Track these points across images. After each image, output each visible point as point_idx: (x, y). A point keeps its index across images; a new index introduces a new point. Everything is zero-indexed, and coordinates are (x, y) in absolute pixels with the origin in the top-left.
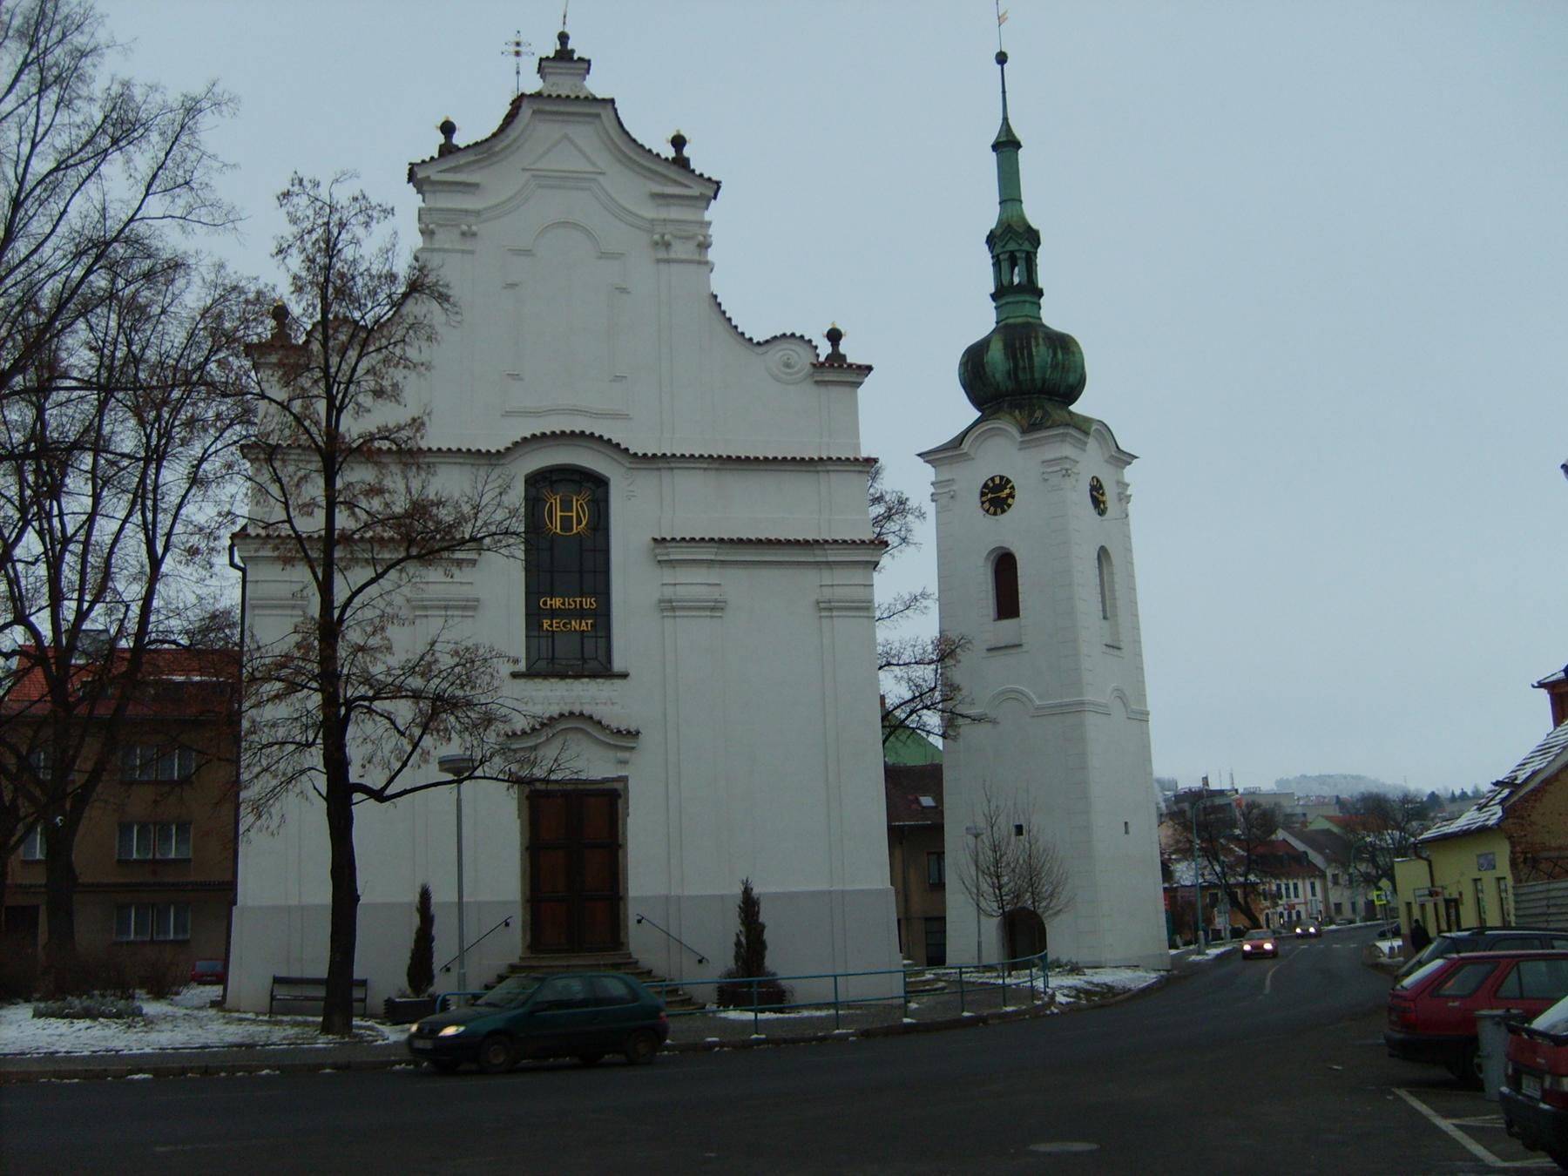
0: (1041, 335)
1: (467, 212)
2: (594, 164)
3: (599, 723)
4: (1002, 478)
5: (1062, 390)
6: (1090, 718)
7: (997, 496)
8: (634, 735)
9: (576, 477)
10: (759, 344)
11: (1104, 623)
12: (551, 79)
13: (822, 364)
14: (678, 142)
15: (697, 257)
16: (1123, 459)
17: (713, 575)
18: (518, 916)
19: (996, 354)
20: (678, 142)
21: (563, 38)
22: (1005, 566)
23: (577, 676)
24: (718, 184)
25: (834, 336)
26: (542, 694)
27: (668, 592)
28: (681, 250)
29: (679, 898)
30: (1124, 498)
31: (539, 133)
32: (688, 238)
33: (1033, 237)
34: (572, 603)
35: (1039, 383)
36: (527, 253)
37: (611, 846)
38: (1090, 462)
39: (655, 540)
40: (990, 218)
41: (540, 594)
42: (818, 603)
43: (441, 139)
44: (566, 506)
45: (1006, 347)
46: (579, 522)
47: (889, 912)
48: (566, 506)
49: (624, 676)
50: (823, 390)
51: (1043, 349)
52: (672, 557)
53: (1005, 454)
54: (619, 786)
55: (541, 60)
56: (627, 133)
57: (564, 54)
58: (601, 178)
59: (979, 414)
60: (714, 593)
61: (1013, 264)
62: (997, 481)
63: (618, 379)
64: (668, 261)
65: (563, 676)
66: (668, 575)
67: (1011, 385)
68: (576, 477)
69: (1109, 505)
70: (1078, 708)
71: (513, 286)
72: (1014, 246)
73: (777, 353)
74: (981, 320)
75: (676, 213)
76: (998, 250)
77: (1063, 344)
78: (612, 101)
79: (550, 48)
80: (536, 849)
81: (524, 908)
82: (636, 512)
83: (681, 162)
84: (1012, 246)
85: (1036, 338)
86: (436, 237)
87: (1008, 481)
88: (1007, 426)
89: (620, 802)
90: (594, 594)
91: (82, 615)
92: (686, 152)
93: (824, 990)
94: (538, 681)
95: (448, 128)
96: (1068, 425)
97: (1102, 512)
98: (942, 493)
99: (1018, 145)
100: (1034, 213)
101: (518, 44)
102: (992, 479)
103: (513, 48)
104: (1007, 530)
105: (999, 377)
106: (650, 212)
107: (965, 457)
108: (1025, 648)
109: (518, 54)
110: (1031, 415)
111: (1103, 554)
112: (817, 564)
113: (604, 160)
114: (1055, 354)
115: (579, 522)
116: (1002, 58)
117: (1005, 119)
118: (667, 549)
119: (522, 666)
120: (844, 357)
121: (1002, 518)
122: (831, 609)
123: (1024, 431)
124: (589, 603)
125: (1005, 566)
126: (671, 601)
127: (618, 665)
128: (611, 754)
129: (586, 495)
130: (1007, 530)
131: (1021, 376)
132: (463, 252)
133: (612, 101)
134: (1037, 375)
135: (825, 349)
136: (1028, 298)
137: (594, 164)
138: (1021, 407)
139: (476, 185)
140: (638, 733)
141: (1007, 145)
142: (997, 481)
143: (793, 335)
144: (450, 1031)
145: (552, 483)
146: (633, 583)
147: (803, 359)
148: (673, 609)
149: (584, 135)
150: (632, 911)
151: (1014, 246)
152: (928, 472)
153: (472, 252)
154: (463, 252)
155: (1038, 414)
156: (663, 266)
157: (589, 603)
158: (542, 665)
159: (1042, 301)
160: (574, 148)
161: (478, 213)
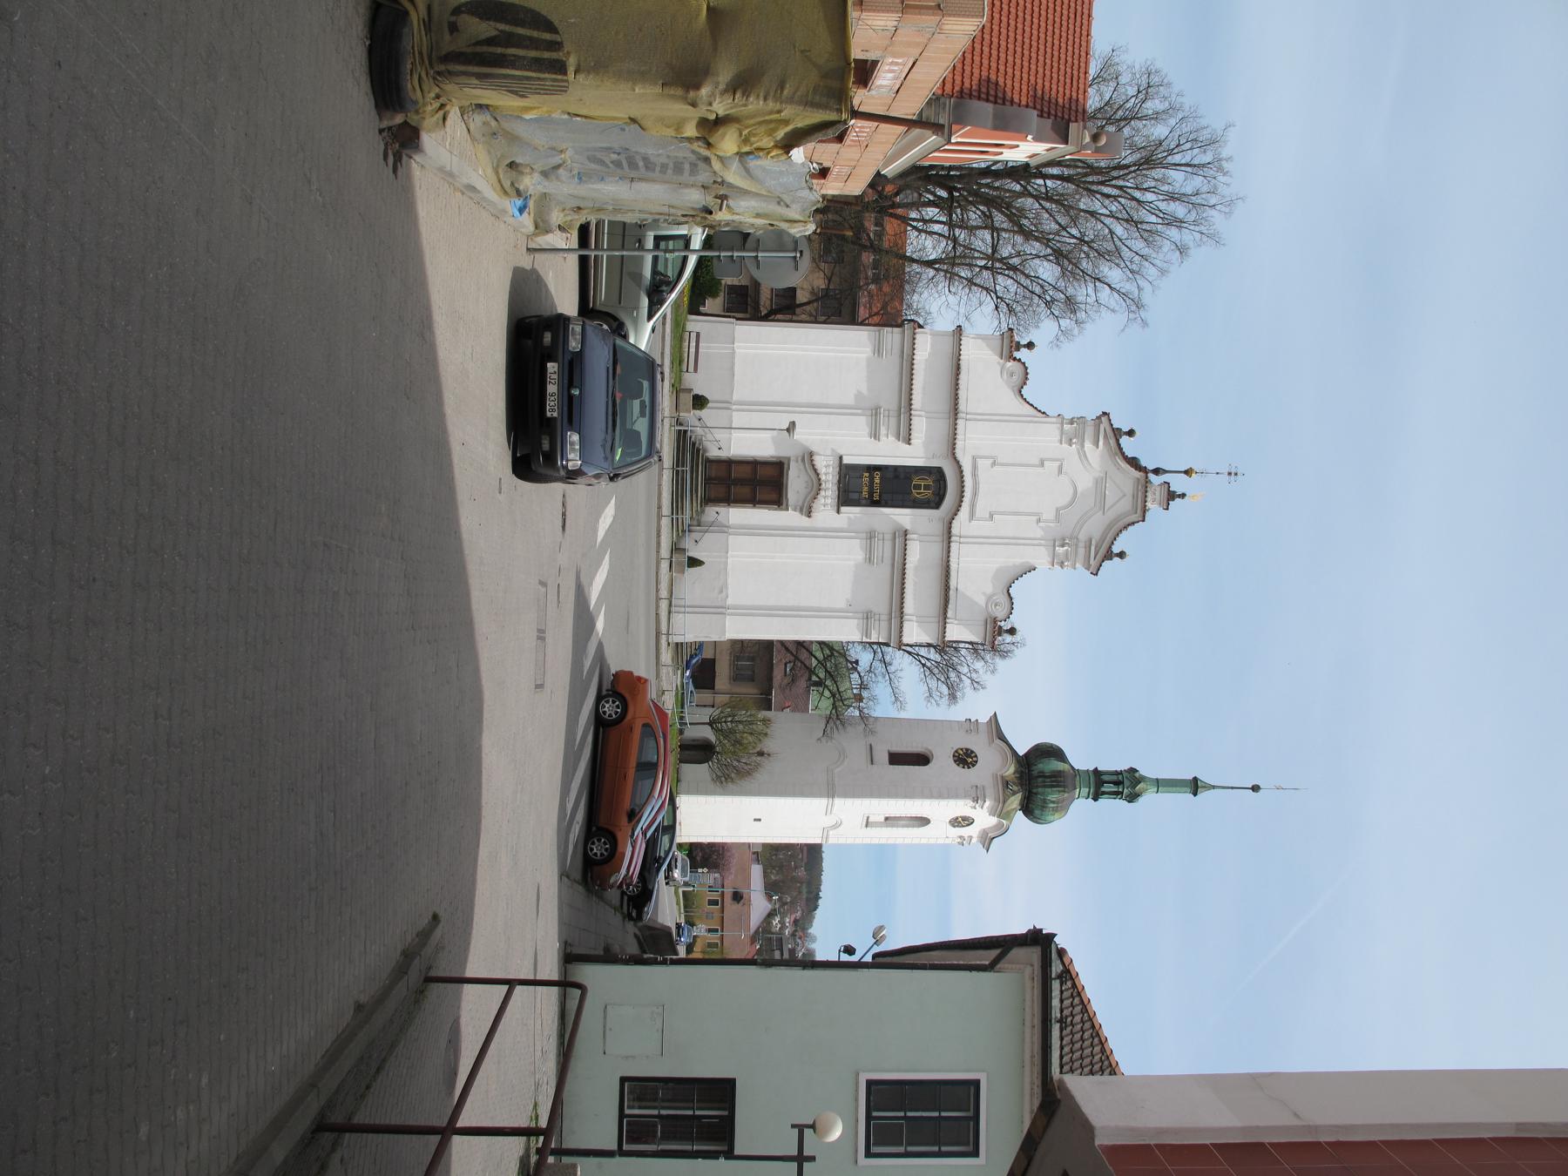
7: (965, 758)
8: (809, 515)
14: (1121, 555)
16: (987, 840)
17: (888, 560)
18: (723, 454)
19: (1060, 766)
22: (922, 759)
33: (1132, 798)
37: (753, 501)
43: (1125, 429)
44: (927, 487)
53: (992, 765)
59: (1021, 751)
66: (888, 536)
67: (1035, 773)
72: (1121, 785)
73: (1004, 599)
74: (1081, 758)
75: (1081, 551)
77: (1062, 808)
80: (755, 464)
83: (1109, 555)
84: (1127, 783)
91: (915, 228)
95: (1131, 433)
98: (971, 726)
105: (1040, 766)
106: (1083, 536)
113: (1111, 515)
116: (1255, 788)
119: (846, 461)
124: (876, 497)
125: (922, 759)
127: (843, 509)
135: (1006, 626)
141: (1195, 786)
144: (144, 1130)
147: (1000, 613)
149: (1125, 505)
151: (1121, 785)
152: (984, 718)
157: (876, 497)
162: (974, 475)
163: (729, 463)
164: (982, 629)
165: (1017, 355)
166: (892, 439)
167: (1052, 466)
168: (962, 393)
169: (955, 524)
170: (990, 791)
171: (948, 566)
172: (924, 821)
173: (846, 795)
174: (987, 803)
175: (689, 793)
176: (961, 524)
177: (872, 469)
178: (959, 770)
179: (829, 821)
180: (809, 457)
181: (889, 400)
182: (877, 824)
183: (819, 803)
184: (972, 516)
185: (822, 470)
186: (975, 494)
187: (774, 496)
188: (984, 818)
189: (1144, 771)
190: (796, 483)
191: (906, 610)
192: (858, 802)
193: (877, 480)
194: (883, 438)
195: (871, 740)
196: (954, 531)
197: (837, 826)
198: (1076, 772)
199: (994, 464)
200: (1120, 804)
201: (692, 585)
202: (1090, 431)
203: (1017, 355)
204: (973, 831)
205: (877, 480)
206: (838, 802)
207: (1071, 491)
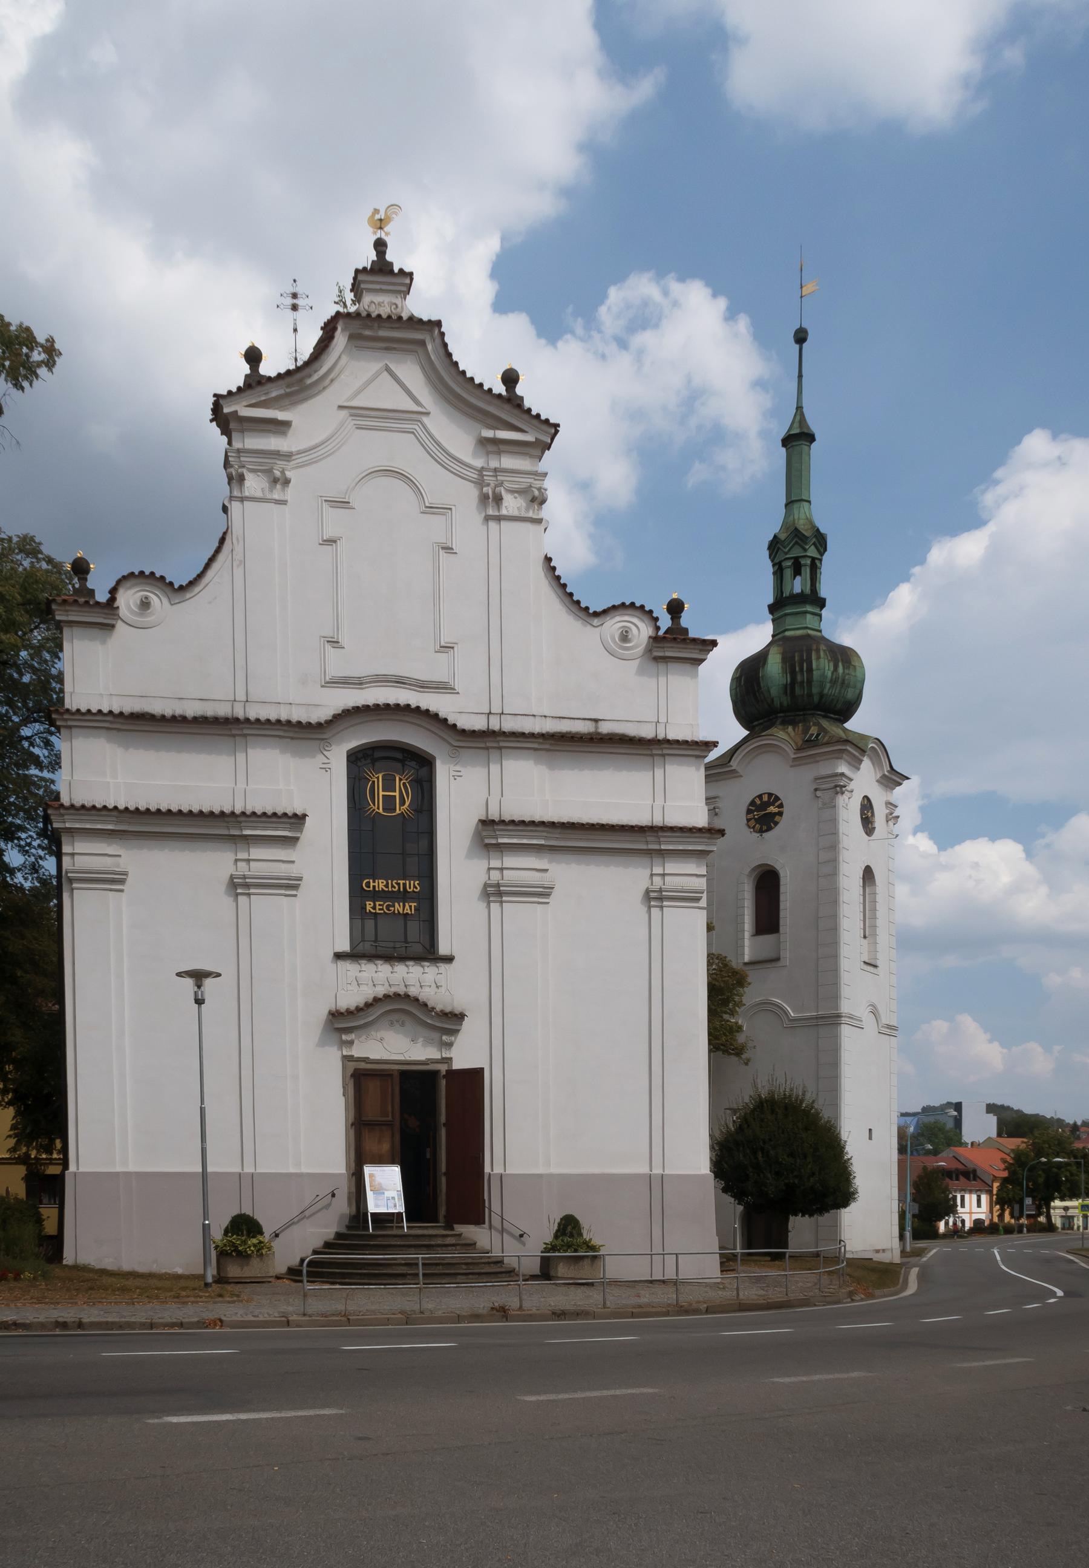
0: (823, 647)
3: (426, 1005)
4: (770, 795)
5: (839, 706)
7: (764, 814)
8: (460, 1017)
9: (399, 756)
11: (865, 942)
13: (663, 639)
14: (510, 378)
19: (774, 666)
20: (510, 378)
21: (380, 246)
24: (556, 426)
25: (675, 608)
27: (495, 876)
28: (512, 504)
33: (821, 542)
35: (816, 699)
36: (344, 504)
43: (246, 369)
44: (389, 785)
45: (784, 660)
46: (403, 803)
48: (389, 785)
49: (449, 959)
50: (662, 666)
52: (501, 841)
53: (774, 773)
55: (357, 271)
61: (797, 571)
62: (765, 798)
63: (447, 648)
64: (499, 519)
67: (786, 701)
69: (876, 825)
71: (331, 541)
73: (614, 625)
77: (844, 656)
78: (439, 324)
79: (367, 257)
81: (349, 1181)
82: (462, 795)
83: (513, 401)
84: (797, 552)
85: (818, 651)
87: (777, 798)
88: (783, 736)
90: (418, 878)
92: (520, 390)
93: (638, 1270)
95: (253, 356)
96: (847, 741)
99: (811, 438)
100: (822, 512)
101: (295, 296)
102: (760, 797)
103: (289, 301)
104: (769, 849)
105: (774, 692)
109: (295, 308)
110: (806, 731)
111: (868, 874)
112: (649, 853)
114: (836, 667)
115: (403, 803)
116: (801, 337)
117: (799, 408)
118: (494, 833)
119: (345, 946)
124: (413, 885)
125: (767, 883)
127: (443, 949)
128: (436, 1035)
130: (769, 849)
131: (798, 691)
133: (439, 324)
134: (815, 690)
135: (665, 622)
136: (809, 608)
138: (794, 723)
139: (287, 424)
142: (765, 798)
145: (374, 761)
147: (642, 631)
155: (814, 730)
156: (492, 525)
157: (413, 885)
158: (367, 947)
159: (824, 612)
161: (288, 456)
162: (358, 683)
165: (102, 597)
167: (334, 522)
168: (191, 710)
170: (824, 769)
171: (543, 736)
173: (835, 997)
174: (843, 768)
176: (462, 709)
177: (358, 895)
179: (868, 1020)
180: (342, 1022)
181: (217, 863)
182: (874, 951)
183: (847, 1033)
184: (443, 687)
185: (367, 993)
186: (400, 682)
188: (863, 780)
189: (773, 526)
190: (395, 1046)
191: (641, 818)
192: (845, 978)
193: (380, 884)
194: (293, 870)
196: (478, 724)
197: (875, 1012)
198: (778, 637)
199: (334, 643)
201: (625, 1252)
202: (253, 442)
203: (102, 597)
205: (380, 884)
206: (845, 1007)
207: (385, 481)
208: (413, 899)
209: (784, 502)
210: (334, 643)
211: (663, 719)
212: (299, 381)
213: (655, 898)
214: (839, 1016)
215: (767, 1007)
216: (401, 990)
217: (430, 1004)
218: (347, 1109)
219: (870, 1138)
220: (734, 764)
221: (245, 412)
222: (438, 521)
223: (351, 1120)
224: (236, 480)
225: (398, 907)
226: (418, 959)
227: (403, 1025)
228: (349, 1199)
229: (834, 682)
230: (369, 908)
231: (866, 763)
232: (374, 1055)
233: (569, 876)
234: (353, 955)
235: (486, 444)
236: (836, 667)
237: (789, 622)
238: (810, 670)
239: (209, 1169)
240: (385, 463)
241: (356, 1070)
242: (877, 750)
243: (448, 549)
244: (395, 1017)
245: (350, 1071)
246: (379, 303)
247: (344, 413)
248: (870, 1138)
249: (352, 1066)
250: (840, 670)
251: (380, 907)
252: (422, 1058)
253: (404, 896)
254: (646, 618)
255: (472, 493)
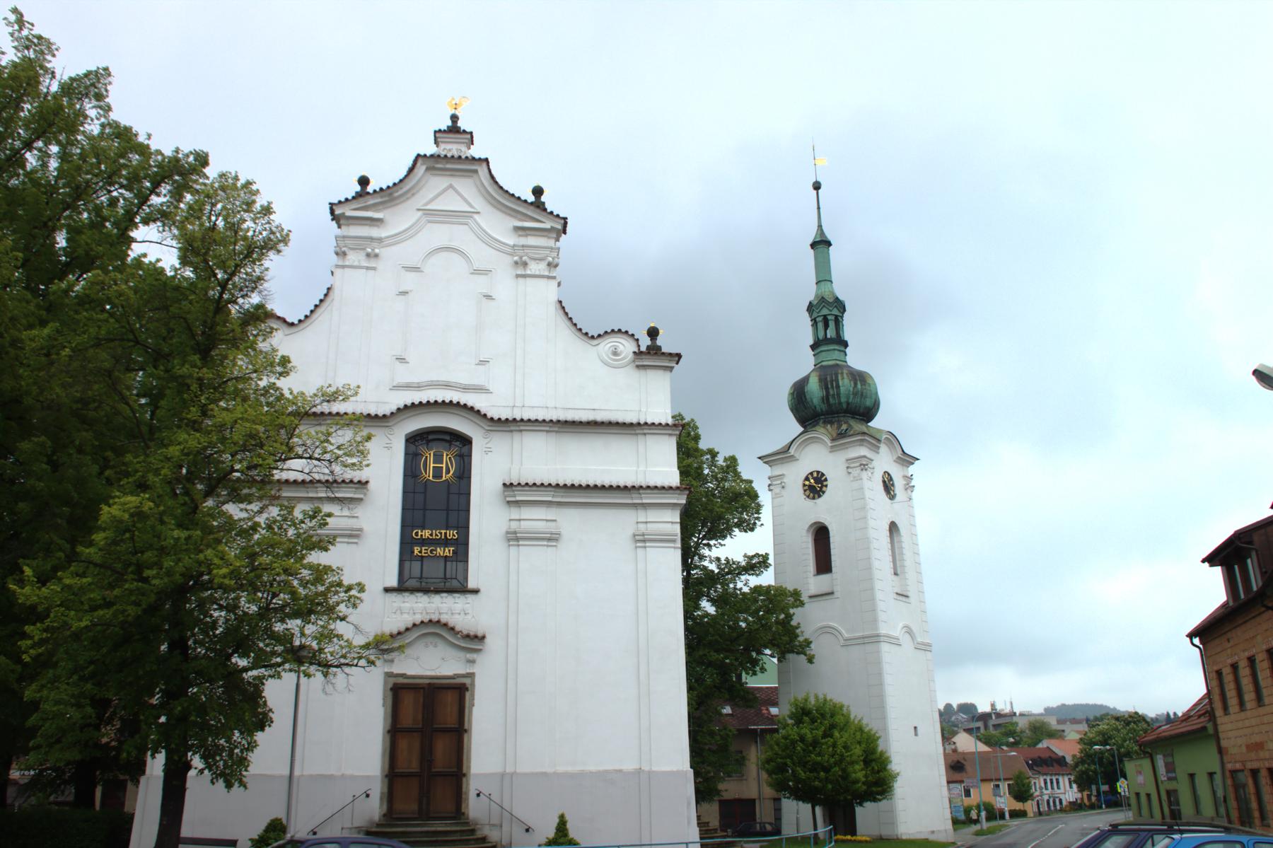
1: (372, 239)
2: (471, 206)
6: (885, 647)
8: (480, 639)
9: (448, 438)
10: (593, 337)
11: (894, 577)
12: (442, 146)
14: (538, 192)
15: (546, 273)
16: (907, 460)
18: (377, 789)
19: (814, 387)
20: (538, 192)
21: (454, 118)
22: (821, 535)
23: (437, 591)
24: (565, 219)
25: (653, 333)
26: (407, 605)
27: (514, 525)
29: (650, 772)
30: (909, 487)
31: (434, 189)
32: (541, 260)
33: (840, 306)
34: (438, 534)
36: (416, 269)
37: (458, 732)
38: (884, 461)
39: (504, 485)
40: (809, 293)
41: (414, 527)
42: (634, 535)
44: (438, 459)
45: (820, 380)
46: (448, 472)
47: (689, 789)
48: (438, 459)
49: (476, 592)
50: (642, 372)
51: (846, 381)
54: (467, 681)
56: (501, 188)
57: (454, 129)
58: (476, 216)
59: (802, 429)
60: (551, 527)
64: (524, 276)
65: (426, 591)
66: (515, 513)
67: (824, 407)
68: (448, 438)
70: (875, 639)
71: (404, 293)
73: (606, 345)
74: (803, 363)
76: (815, 315)
77: (860, 378)
78: (486, 160)
79: (446, 123)
80: (395, 732)
82: (491, 465)
83: (539, 205)
84: (825, 312)
86: (348, 257)
88: (823, 433)
89: (468, 695)
90: (457, 528)
94: (406, 594)
95: (364, 181)
97: (892, 497)
99: (829, 244)
104: (821, 510)
105: (816, 401)
106: (511, 240)
107: (792, 459)
108: (836, 595)
111: (893, 527)
112: (635, 506)
113: (479, 203)
114: (856, 384)
115: (448, 472)
116: (817, 186)
117: (820, 226)
118: (515, 492)
119: (393, 582)
120: (659, 348)
121: (819, 501)
122: (644, 541)
123: (833, 440)
124: (452, 534)
125: (821, 535)
126: (515, 533)
127: (471, 584)
128: (461, 654)
129: (455, 450)
131: (831, 400)
132: (368, 268)
134: (843, 400)
135: (645, 342)
136: (836, 347)
137: (471, 206)
138: (831, 423)
140: (484, 637)
143: (620, 331)
145: (428, 442)
146: (487, 518)
147: (627, 347)
148: (517, 539)
150: (473, 786)
153: (374, 269)
154: (368, 268)
155: (844, 427)
156: (521, 280)
157: (452, 534)
158: (412, 583)
159: (848, 350)
160: (459, 194)
161: (380, 240)
162: (418, 387)
163: (394, 775)
164: (652, 374)
166: (358, 511)
167: (409, 280)
169: (494, 413)
172: (1148, 795)
175: (893, 823)
177: (407, 543)
178: (829, 491)
179: (905, 640)
186: (447, 386)
187: (450, 698)
192: (881, 606)
193: (426, 534)
195: (804, 598)
197: (909, 631)
200: (847, 320)
204: (897, 473)
205: (426, 534)
207: (444, 254)
208: (451, 545)
209: (815, 281)
210: (402, 360)
211: (643, 410)
212: (390, 194)
213: (641, 540)
214: (875, 639)
215: (827, 630)
216: (435, 618)
217: (458, 628)
218: (385, 719)
219: (916, 734)
220: (792, 451)
221: (349, 213)
222: (481, 279)
223: (388, 727)
224: (341, 254)
225: (440, 551)
226: (451, 591)
227: (436, 646)
228: (381, 799)
229: (855, 394)
230: (416, 552)
231: (884, 448)
232: (410, 672)
233: (569, 521)
234: (401, 588)
235: (517, 229)
236: (856, 384)
237: (823, 356)
238: (838, 387)
239: (297, 773)
240: (445, 243)
241: (395, 684)
242: (893, 440)
243: (488, 297)
244: (430, 639)
245: (390, 686)
246: (452, 148)
247: (420, 213)
248: (916, 734)
249: (392, 681)
250: (859, 386)
251: (425, 551)
252: (450, 673)
253: (446, 542)
254: (631, 340)
255: (509, 260)
